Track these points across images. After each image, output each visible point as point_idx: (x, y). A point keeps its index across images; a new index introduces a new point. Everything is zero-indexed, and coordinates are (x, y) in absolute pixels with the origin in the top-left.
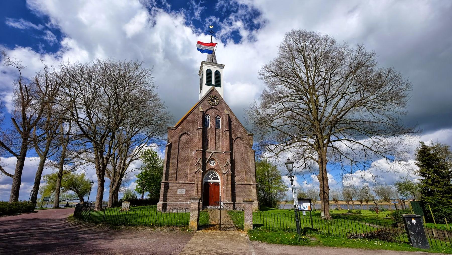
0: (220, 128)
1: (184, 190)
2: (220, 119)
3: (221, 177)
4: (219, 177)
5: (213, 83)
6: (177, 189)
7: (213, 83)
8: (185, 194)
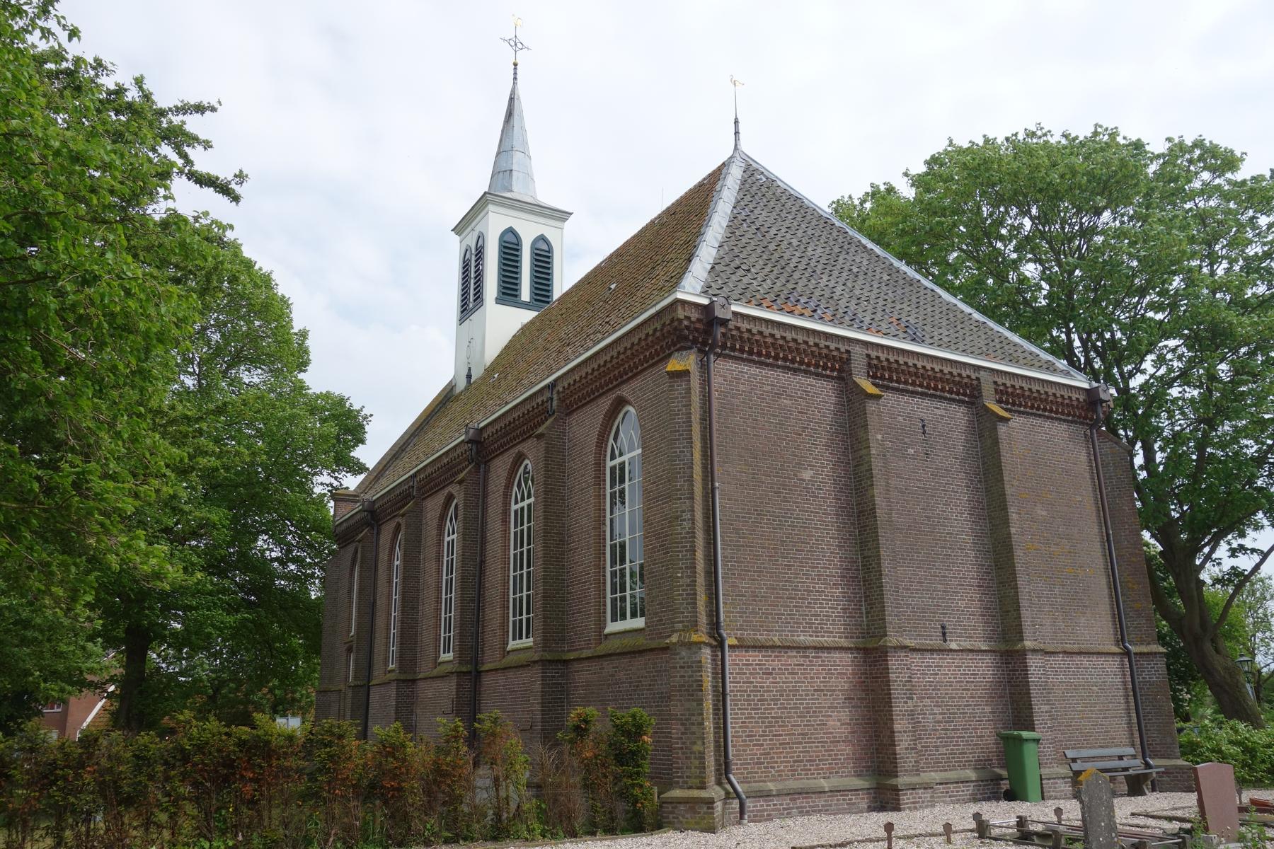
5: (525, 294)
7: (525, 294)
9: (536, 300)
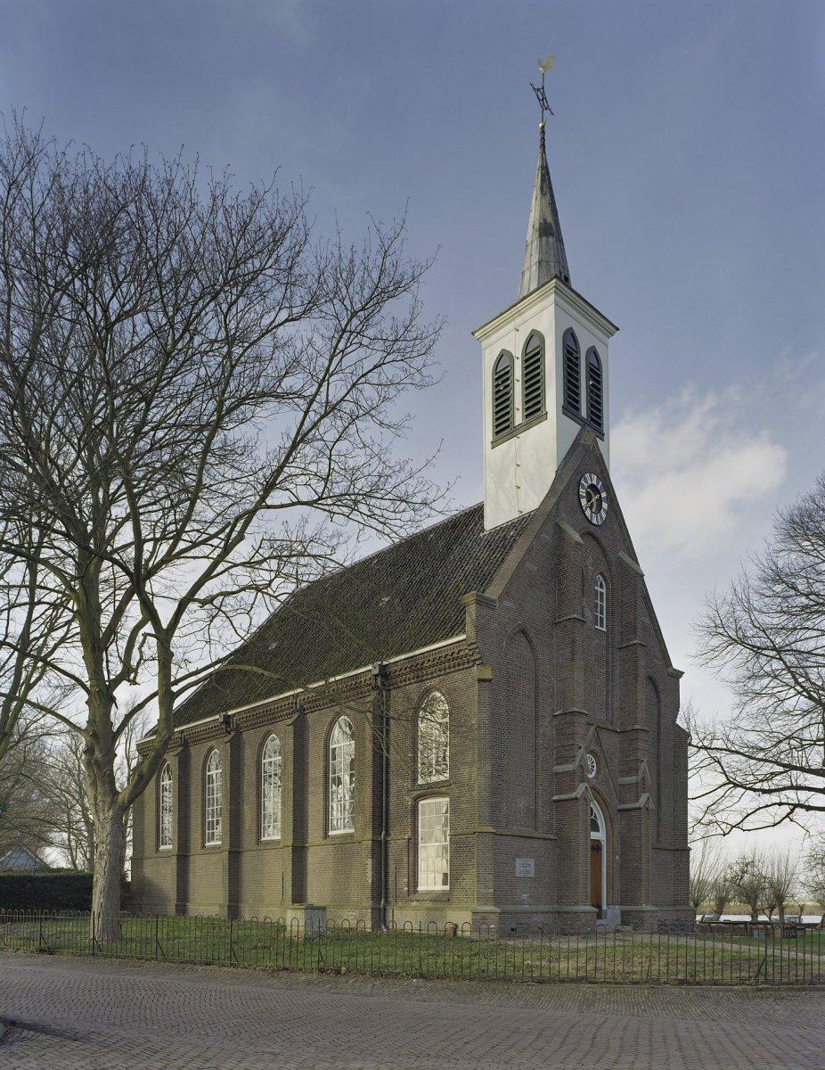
0: (604, 629)
1: (532, 862)
2: (604, 591)
3: (610, 821)
4: (601, 822)
6: (514, 859)
8: (534, 879)
9: (592, 419)
